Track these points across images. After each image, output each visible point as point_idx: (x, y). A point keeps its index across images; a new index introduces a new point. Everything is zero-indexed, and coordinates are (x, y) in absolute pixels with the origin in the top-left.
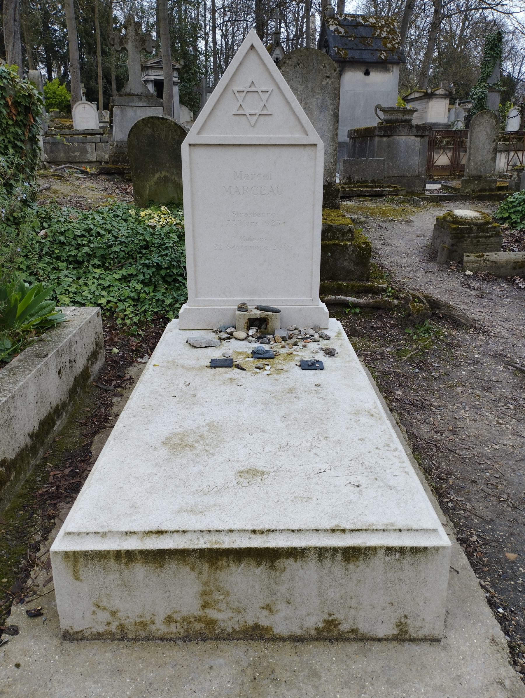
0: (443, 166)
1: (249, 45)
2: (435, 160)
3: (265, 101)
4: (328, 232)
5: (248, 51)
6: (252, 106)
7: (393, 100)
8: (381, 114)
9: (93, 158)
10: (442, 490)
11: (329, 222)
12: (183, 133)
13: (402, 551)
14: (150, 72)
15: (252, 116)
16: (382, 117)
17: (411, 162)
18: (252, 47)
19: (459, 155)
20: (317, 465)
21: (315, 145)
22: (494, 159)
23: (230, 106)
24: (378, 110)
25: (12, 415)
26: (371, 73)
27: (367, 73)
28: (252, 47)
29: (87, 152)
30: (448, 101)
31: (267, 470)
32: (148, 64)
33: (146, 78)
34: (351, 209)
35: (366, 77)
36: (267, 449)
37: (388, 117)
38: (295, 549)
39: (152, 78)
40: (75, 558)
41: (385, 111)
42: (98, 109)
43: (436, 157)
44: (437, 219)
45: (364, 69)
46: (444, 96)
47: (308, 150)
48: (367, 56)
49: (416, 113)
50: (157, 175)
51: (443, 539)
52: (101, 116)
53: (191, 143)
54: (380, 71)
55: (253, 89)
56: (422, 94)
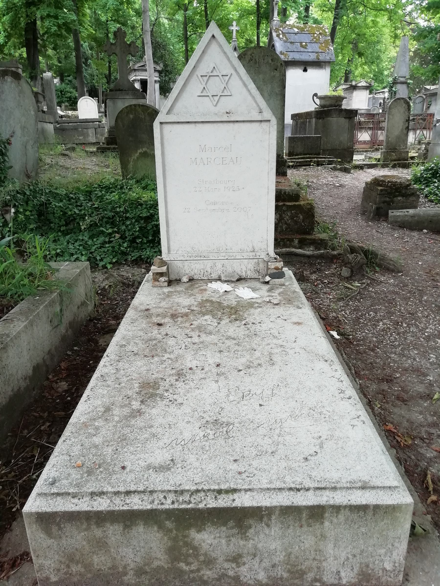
0: (365, 141)
1: (211, 35)
2: (358, 137)
3: (225, 84)
4: (280, 196)
5: (210, 40)
6: (215, 85)
7: (326, 90)
8: (318, 101)
9: (92, 139)
10: (400, 443)
11: (280, 188)
12: (154, 113)
13: (363, 508)
14: (137, 73)
15: (214, 97)
16: (318, 103)
17: (341, 138)
18: (213, 36)
19: (377, 133)
20: (279, 415)
21: (269, 121)
22: (407, 135)
23: (195, 87)
24: (315, 98)
25: (3, 364)
26: (308, 70)
27: (305, 70)
28: (213, 36)
29: (88, 135)
30: (368, 91)
31: (231, 421)
32: (136, 67)
33: (134, 78)
34: (294, 175)
35: (305, 73)
36: (231, 398)
37: (323, 102)
38: (259, 508)
39: (139, 78)
40: (45, 519)
41: (321, 98)
42: (98, 102)
43: (359, 135)
44: (366, 183)
45: (303, 68)
46: (366, 88)
47: (264, 125)
48: (305, 57)
49: (345, 100)
50: (139, 151)
51: (404, 497)
52: (99, 107)
53: (162, 121)
54: (315, 68)
55: (215, 73)
56: (349, 86)
